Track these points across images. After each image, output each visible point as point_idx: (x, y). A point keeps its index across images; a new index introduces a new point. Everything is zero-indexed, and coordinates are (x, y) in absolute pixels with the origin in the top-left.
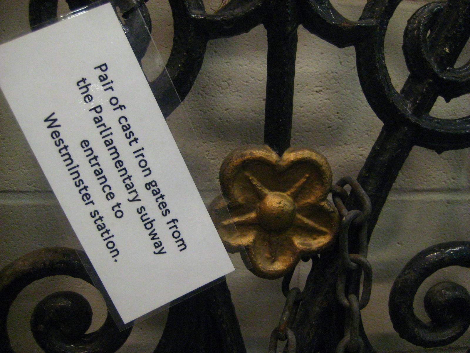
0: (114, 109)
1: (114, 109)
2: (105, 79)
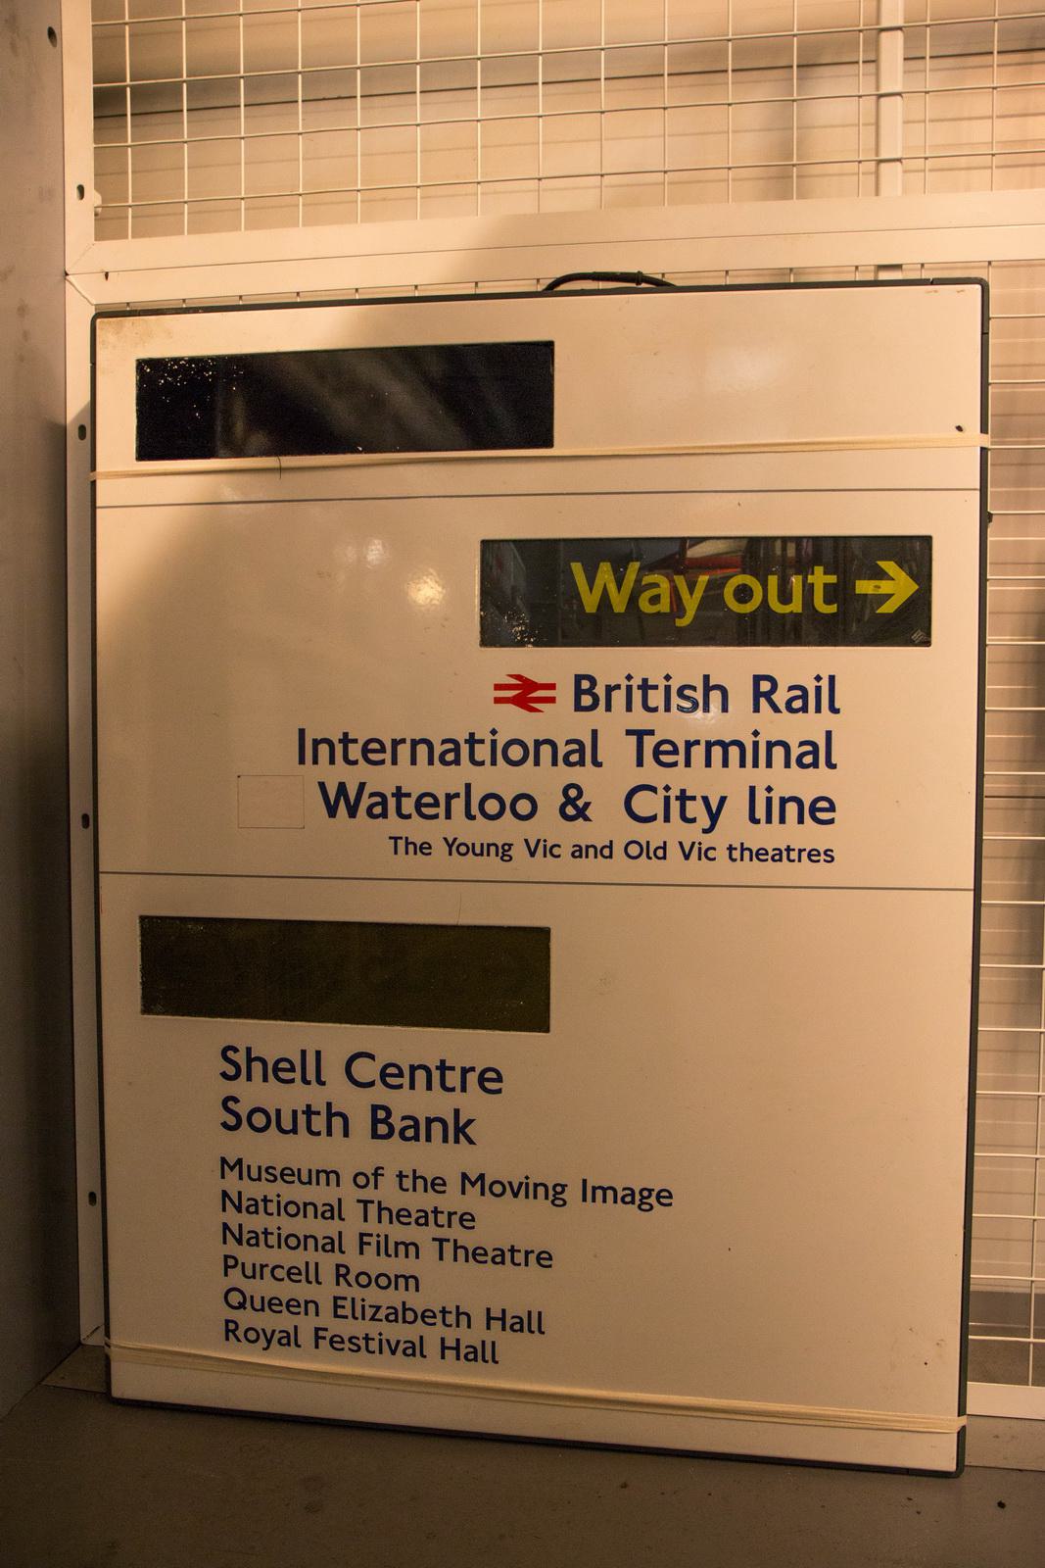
0: (376, 1187)
1: (376, 1187)
2: (804, 697)
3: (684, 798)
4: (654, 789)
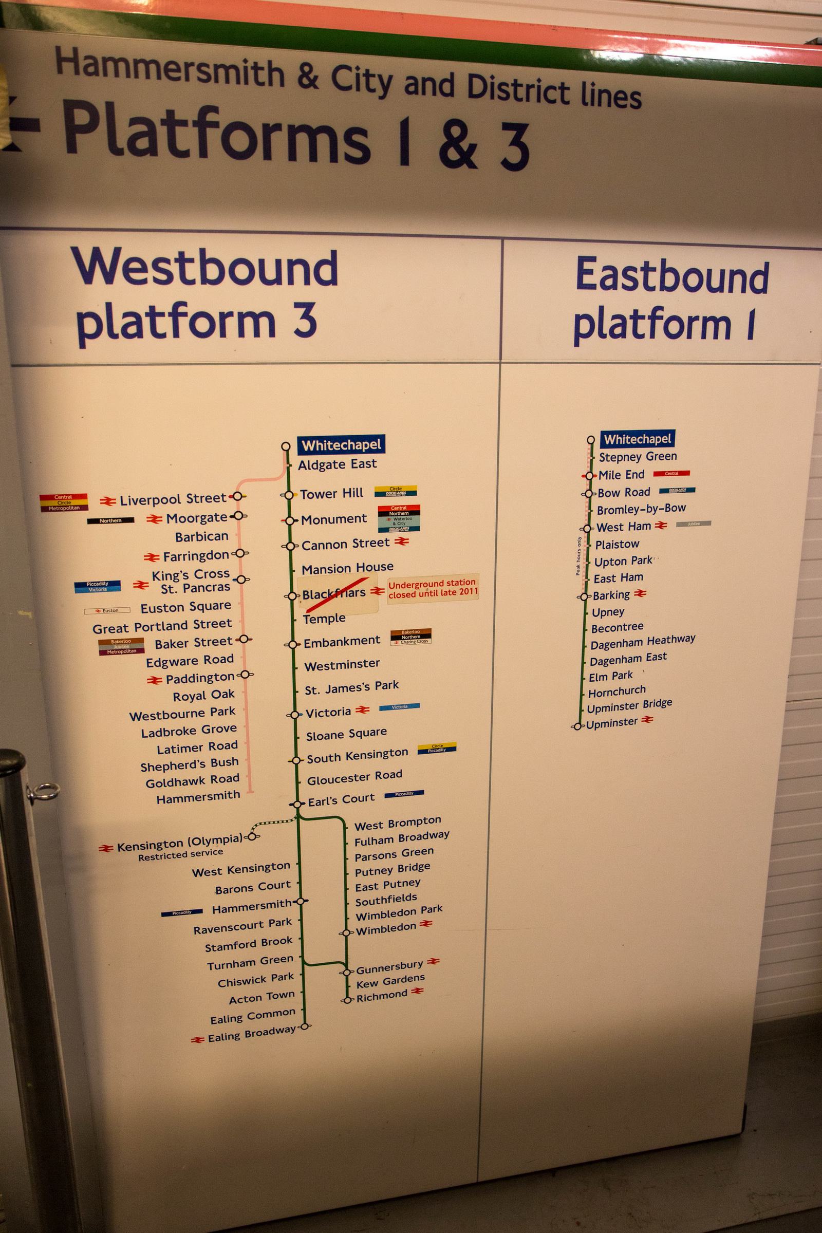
3: (368, 75)
4: (349, 68)
